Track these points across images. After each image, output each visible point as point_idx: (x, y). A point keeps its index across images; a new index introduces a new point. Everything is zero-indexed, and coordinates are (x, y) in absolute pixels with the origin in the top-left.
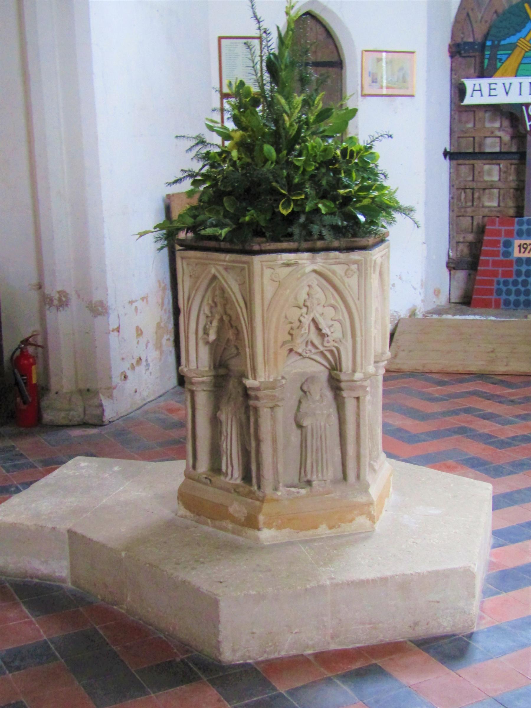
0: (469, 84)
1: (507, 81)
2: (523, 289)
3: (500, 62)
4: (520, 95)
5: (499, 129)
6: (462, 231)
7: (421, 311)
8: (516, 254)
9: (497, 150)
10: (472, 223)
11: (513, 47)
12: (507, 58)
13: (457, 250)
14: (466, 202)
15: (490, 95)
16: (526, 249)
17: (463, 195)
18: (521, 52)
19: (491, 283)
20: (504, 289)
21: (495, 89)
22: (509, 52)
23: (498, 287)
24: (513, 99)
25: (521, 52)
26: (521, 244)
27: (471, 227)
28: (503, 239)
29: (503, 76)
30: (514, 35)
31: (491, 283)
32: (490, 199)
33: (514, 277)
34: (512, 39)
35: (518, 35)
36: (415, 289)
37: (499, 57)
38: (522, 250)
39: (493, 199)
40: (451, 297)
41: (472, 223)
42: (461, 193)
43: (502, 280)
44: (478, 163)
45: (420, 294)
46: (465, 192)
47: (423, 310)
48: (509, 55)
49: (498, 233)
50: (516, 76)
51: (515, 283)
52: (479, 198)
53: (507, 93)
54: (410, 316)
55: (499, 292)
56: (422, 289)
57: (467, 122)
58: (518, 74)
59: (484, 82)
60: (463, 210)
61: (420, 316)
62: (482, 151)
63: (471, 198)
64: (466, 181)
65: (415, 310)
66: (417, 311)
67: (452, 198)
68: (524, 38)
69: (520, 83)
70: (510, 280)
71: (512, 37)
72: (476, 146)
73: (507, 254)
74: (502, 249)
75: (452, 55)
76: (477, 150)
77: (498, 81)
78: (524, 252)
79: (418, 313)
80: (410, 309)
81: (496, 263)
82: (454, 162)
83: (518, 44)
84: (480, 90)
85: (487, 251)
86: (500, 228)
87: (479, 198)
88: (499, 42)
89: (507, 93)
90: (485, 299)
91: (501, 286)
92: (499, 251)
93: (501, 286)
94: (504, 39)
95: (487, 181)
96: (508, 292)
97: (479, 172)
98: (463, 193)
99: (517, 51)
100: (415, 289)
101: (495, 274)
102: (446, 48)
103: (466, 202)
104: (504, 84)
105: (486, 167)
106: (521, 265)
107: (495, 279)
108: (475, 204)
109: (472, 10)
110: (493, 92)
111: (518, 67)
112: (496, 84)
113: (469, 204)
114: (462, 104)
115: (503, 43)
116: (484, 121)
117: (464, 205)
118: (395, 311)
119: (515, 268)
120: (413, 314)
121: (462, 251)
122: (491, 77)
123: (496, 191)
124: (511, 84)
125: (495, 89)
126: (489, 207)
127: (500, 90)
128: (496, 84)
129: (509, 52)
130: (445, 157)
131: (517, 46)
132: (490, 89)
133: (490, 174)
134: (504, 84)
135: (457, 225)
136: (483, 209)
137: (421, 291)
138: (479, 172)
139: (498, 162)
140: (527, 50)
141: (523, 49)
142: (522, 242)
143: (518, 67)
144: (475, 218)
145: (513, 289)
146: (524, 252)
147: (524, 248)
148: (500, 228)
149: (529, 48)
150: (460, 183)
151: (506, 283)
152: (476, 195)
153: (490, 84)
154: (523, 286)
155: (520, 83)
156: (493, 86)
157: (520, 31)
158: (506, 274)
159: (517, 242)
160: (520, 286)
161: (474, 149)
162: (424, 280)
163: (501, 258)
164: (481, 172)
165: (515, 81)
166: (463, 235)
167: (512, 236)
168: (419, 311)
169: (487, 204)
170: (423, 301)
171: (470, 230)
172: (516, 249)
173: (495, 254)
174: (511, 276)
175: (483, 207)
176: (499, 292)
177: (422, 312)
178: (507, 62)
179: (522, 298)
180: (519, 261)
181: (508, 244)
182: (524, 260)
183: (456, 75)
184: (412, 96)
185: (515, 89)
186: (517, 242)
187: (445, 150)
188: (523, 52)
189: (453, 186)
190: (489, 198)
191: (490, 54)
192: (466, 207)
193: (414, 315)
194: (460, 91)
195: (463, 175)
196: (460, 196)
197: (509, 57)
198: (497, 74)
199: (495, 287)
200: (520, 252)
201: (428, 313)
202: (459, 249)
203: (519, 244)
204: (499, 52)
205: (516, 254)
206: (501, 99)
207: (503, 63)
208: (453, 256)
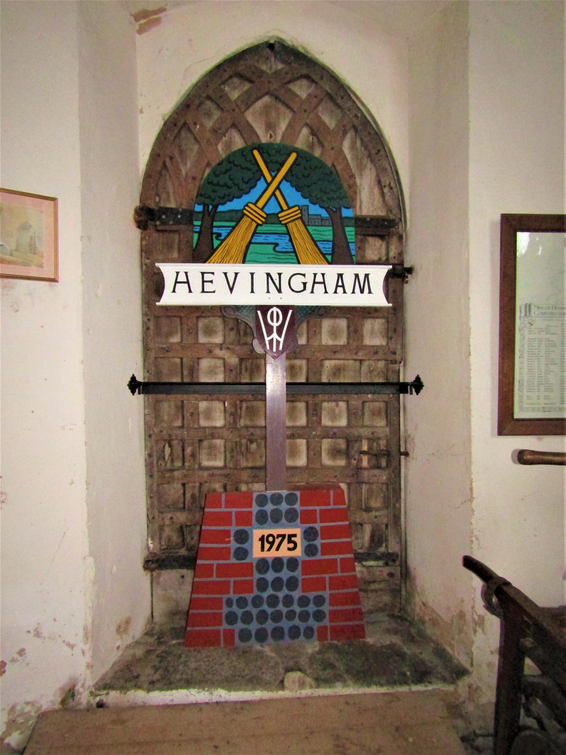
0: (169, 270)
1: (231, 268)
2: (269, 610)
3: (217, 238)
4: (252, 291)
5: (221, 347)
6: (168, 507)
7: (86, 686)
8: (257, 553)
9: (220, 378)
10: (184, 494)
11: (237, 217)
12: (229, 234)
13: (160, 538)
14: (172, 461)
15: (203, 291)
16: (272, 544)
17: (167, 450)
18: (250, 225)
19: (217, 603)
20: (239, 612)
21: (211, 282)
22: (233, 224)
23: (230, 609)
24: (242, 297)
25: (250, 225)
26: (263, 536)
27: (182, 500)
28: (233, 529)
29: (222, 261)
30: (239, 197)
31: (217, 603)
32: (212, 454)
33: (256, 592)
34: (236, 205)
35: (246, 199)
36: (72, 646)
37: (215, 230)
38: (267, 546)
39: (215, 455)
40: (155, 614)
41: (184, 494)
42: (164, 446)
43: (234, 597)
44: (190, 399)
45: (83, 653)
46: (170, 446)
47: (90, 682)
48: (234, 228)
49: (225, 519)
50: (244, 262)
51: (257, 601)
52: (193, 455)
53: (231, 290)
54: (63, 702)
55: (231, 618)
56: (86, 643)
57: (170, 334)
58: (247, 259)
59: (194, 270)
60: (167, 475)
61: (84, 698)
62: (196, 381)
63: (181, 455)
64: (172, 428)
65: (74, 686)
66: (78, 688)
67: (150, 455)
68: (255, 204)
69: (252, 274)
70: (249, 597)
71: (235, 200)
72: (185, 373)
73: (243, 553)
74: (234, 545)
75: (142, 224)
76: (186, 380)
77: (216, 269)
78: (269, 549)
79: (81, 690)
80: (62, 689)
81: (223, 570)
82: (152, 397)
83: (245, 211)
84: (188, 282)
85: (207, 549)
86: (228, 510)
87: (193, 455)
88: (215, 207)
89: (231, 290)
90: (207, 593)
91: (235, 608)
92: (228, 549)
93: (235, 608)
94: (223, 204)
95: (204, 428)
96: (247, 617)
97: (192, 414)
98: (167, 446)
99: (245, 222)
100: (72, 646)
101: (223, 587)
102: (131, 214)
103: (172, 461)
104: (225, 274)
105: (203, 405)
106: (266, 571)
107: (225, 597)
108: (295, 110)
109: (171, 158)
110: (208, 287)
111: (247, 247)
112: (213, 273)
113: (178, 464)
114: (157, 304)
115: (221, 208)
116: (197, 334)
117: (169, 465)
118: (27, 703)
119: (257, 576)
120: (70, 693)
121: (169, 538)
122: (205, 262)
123: (219, 442)
124: (236, 274)
125: (211, 282)
126: (208, 468)
127: (220, 283)
128: (213, 273)
129: (233, 224)
130: (133, 392)
131: (245, 214)
132: (203, 282)
133: (208, 415)
134: (225, 274)
135: (160, 497)
136: (200, 473)
137: (86, 648)
138: (192, 414)
139: (221, 397)
140: (260, 223)
141: (252, 220)
142: (266, 532)
143: (247, 247)
144: (187, 486)
145: (255, 612)
146: (269, 549)
147: (268, 541)
148: (228, 510)
149: (264, 220)
150: (161, 431)
151: (242, 602)
152: (189, 450)
153: (203, 274)
154: (270, 605)
155: (252, 274)
156: (207, 277)
157: (248, 193)
158: (241, 587)
159: (257, 533)
160: (265, 607)
161: (182, 378)
162: (90, 627)
163: (233, 560)
164: (195, 414)
165: (245, 270)
166: (169, 515)
167: (249, 523)
168: (83, 686)
169: (206, 463)
170: (89, 666)
171: (181, 506)
172: (257, 544)
173: (224, 554)
174: (251, 591)
175: (201, 468)
176: (231, 618)
177: (89, 687)
178: (230, 240)
179: (269, 625)
180: (263, 564)
181: (243, 537)
182: (270, 562)
183: (148, 259)
184: (54, 280)
185: (243, 282)
186: (257, 533)
187: (133, 378)
188: (254, 225)
189: (150, 436)
190: (209, 454)
191: (201, 226)
192: (172, 470)
193: (73, 696)
194: (154, 285)
195: (166, 418)
196: (163, 452)
197: (231, 231)
198: (217, 255)
199: (225, 610)
200: (263, 549)
201: (98, 689)
202: (165, 535)
203: (260, 536)
204: (215, 224)
205: (257, 553)
206: (221, 297)
207: (223, 241)
208: (154, 549)
